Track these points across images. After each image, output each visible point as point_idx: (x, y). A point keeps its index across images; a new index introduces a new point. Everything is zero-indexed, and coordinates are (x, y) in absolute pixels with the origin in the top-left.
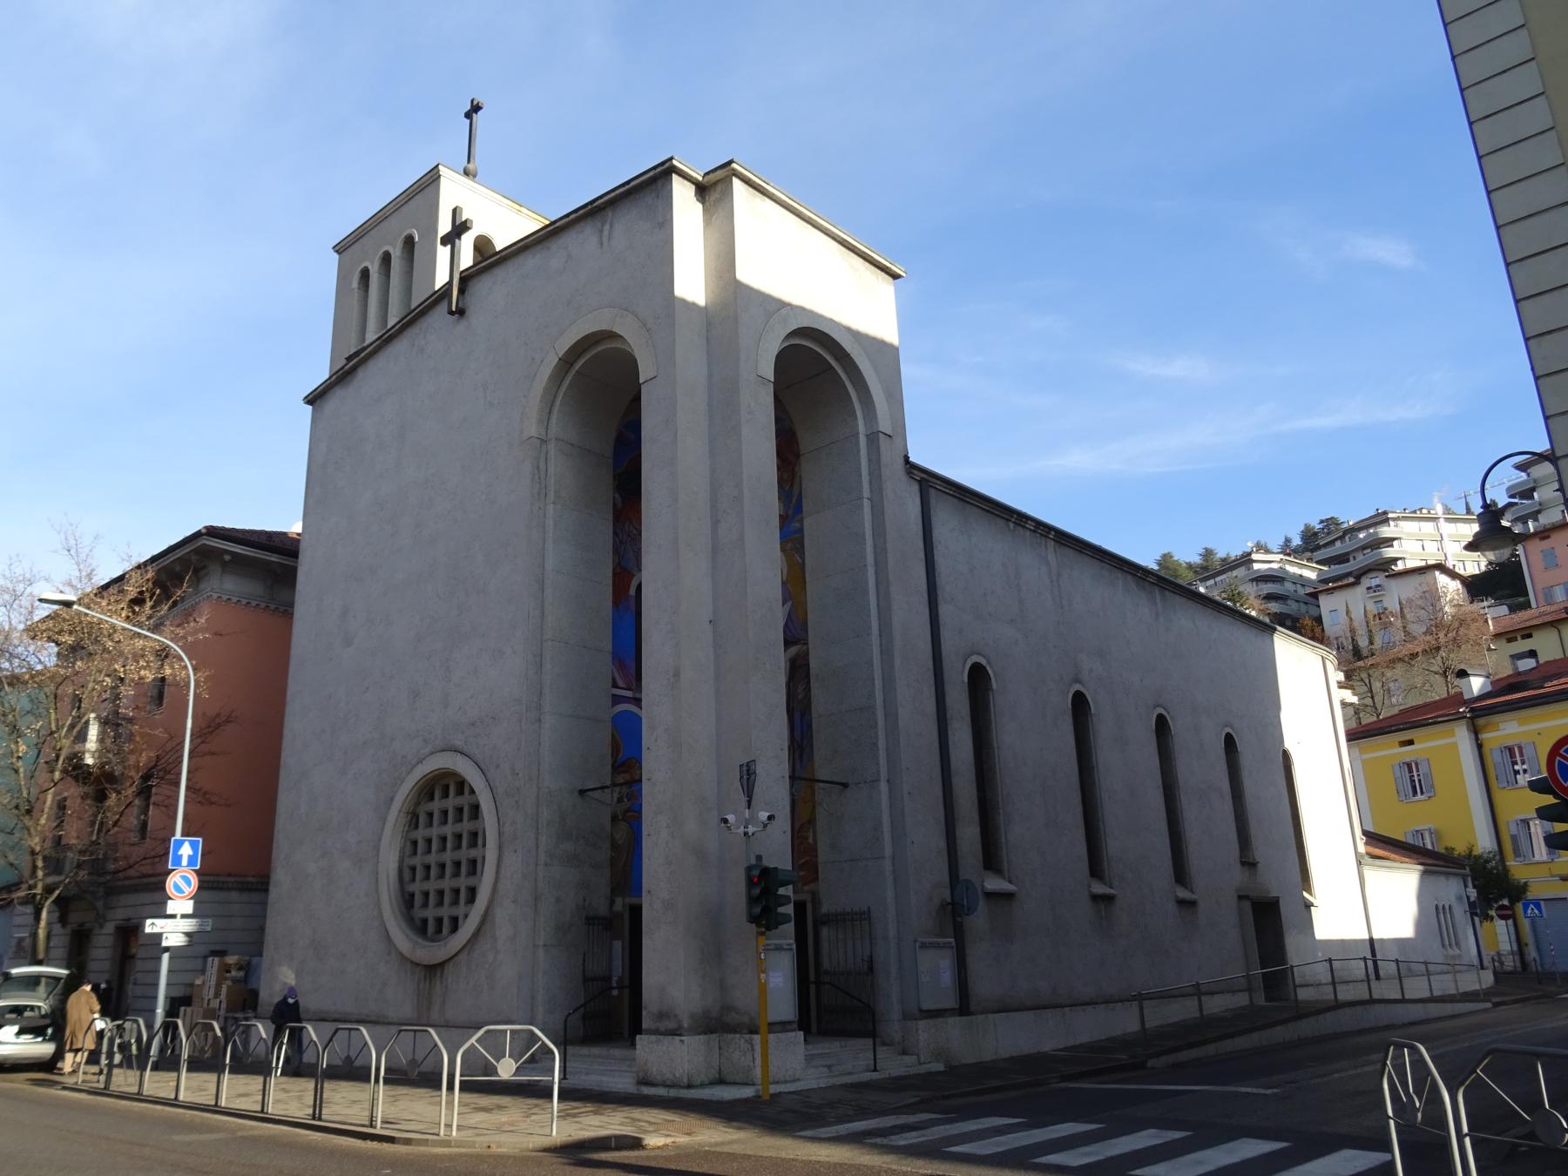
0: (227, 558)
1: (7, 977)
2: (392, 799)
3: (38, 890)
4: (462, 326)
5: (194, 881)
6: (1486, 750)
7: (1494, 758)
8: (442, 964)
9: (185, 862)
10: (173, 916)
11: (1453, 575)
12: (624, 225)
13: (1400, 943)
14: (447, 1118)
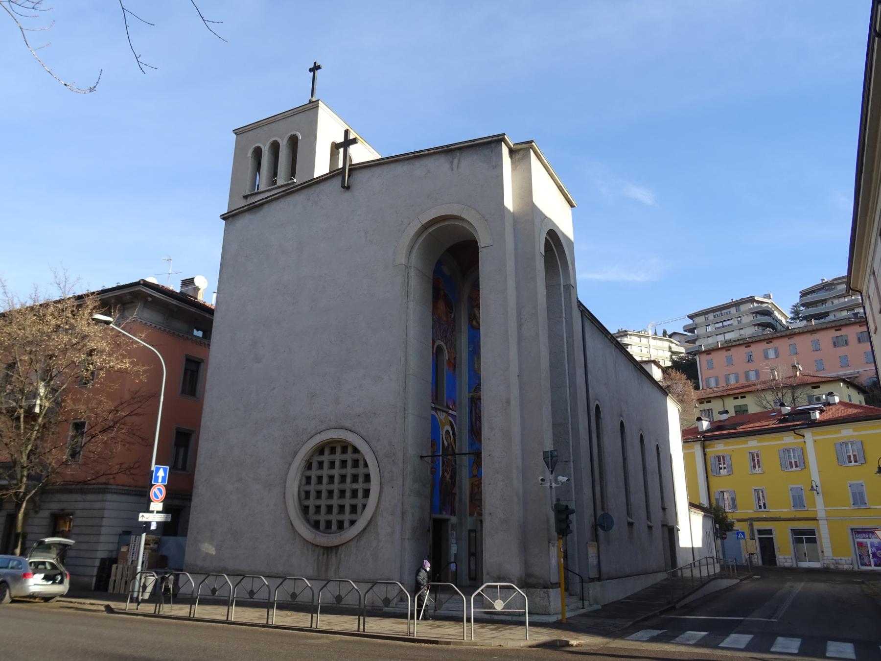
0: (150, 299)
1: (41, 543)
2: (296, 453)
3: (22, 490)
4: (347, 195)
5: (164, 492)
6: (708, 457)
7: (711, 460)
8: (337, 547)
9: (160, 480)
10: (152, 512)
11: (659, 366)
12: (468, 163)
13: (699, 548)
14: (471, 635)
